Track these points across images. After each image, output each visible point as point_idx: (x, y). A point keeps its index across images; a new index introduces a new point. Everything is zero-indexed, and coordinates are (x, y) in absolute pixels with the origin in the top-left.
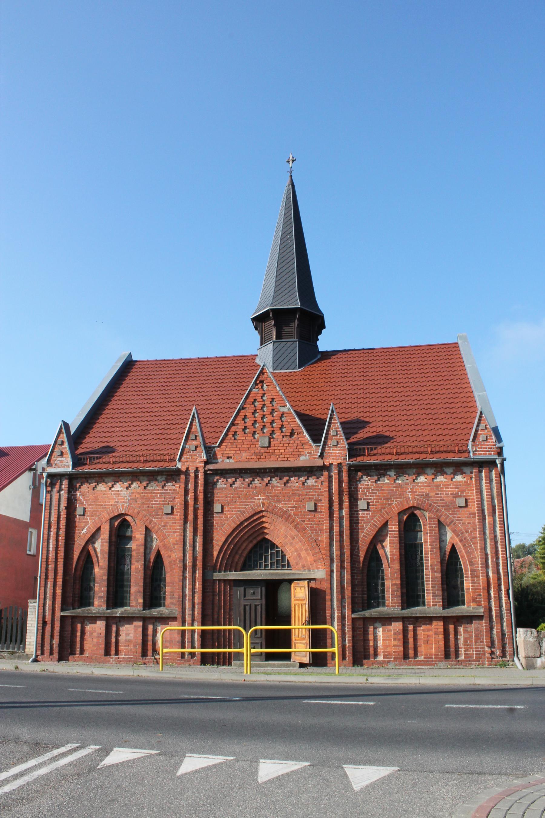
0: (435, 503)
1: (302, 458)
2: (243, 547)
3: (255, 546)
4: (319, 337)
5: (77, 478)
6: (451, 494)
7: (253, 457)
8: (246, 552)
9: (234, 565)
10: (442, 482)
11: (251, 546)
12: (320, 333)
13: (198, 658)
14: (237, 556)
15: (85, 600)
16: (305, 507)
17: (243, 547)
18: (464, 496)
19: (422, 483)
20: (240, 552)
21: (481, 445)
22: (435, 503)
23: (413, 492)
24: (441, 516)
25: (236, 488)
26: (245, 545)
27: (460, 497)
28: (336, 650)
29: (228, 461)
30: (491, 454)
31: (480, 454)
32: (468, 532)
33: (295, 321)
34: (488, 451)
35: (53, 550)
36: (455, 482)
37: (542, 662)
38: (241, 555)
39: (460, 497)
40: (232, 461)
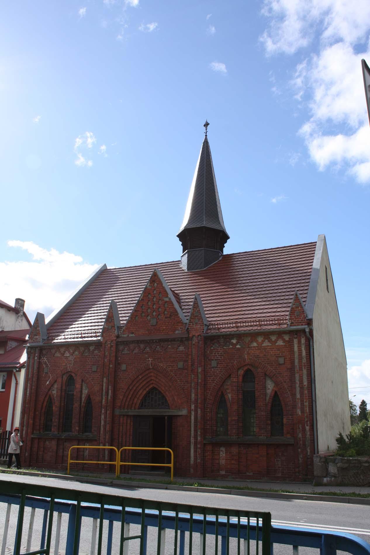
0: (263, 362)
1: (177, 332)
2: (139, 393)
3: (148, 393)
4: (225, 245)
5: (45, 349)
6: (275, 355)
7: (147, 332)
8: (142, 396)
9: (134, 405)
10: (268, 346)
11: (145, 392)
12: (226, 242)
13: (118, 469)
14: (136, 399)
15: (47, 427)
16: (177, 366)
17: (139, 393)
18: (283, 356)
19: (255, 347)
20: (138, 396)
21: (296, 319)
22: (263, 362)
23: (248, 354)
24: (267, 371)
25: (135, 353)
26: (141, 392)
27: (281, 357)
28: (171, 465)
29: (131, 335)
30: (302, 325)
31: (295, 325)
32: (285, 382)
33: (204, 236)
34: (301, 322)
35: (270, 398)
36: (277, 346)
37: (327, 481)
38: (138, 399)
39: (281, 357)
40: (133, 335)
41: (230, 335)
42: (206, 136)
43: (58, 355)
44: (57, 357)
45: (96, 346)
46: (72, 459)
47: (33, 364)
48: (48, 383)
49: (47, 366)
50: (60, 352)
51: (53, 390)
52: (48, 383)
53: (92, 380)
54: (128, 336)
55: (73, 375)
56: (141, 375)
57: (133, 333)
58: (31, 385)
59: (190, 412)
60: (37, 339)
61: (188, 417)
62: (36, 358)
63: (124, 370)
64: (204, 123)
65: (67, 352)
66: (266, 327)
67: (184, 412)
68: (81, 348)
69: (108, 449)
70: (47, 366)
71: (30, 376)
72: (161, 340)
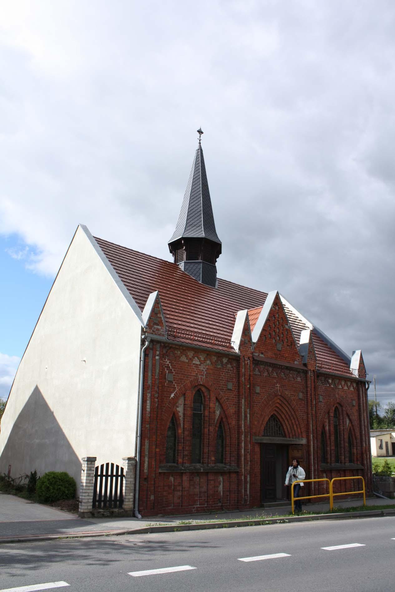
1: (296, 362)
28: (363, 491)
41: (329, 375)
42: (200, 143)
43: (184, 359)
44: (183, 362)
45: (229, 359)
46: (362, 493)
47: (154, 365)
48: (172, 395)
49: (170, 372)
50: (187, 356)
51: (178, 407)
52: (172, 395)
53: (227, 399)
54: (259, 355)
55: (203, 389)
56: (316, 404)
57: (262, 353)
58: (152, 397)
59: (308, 441)
60: (158, 330)
61: (308, 445)
62: (157, 358)
63: (258, 393)
64: (203, 131)
65: (196, 358)
66: (325, 370)
67: (304, 441)
68: (213, 357)
69: (315, 482)
70: (170, 372)
71: (150, 382)
72: (287, 368)
